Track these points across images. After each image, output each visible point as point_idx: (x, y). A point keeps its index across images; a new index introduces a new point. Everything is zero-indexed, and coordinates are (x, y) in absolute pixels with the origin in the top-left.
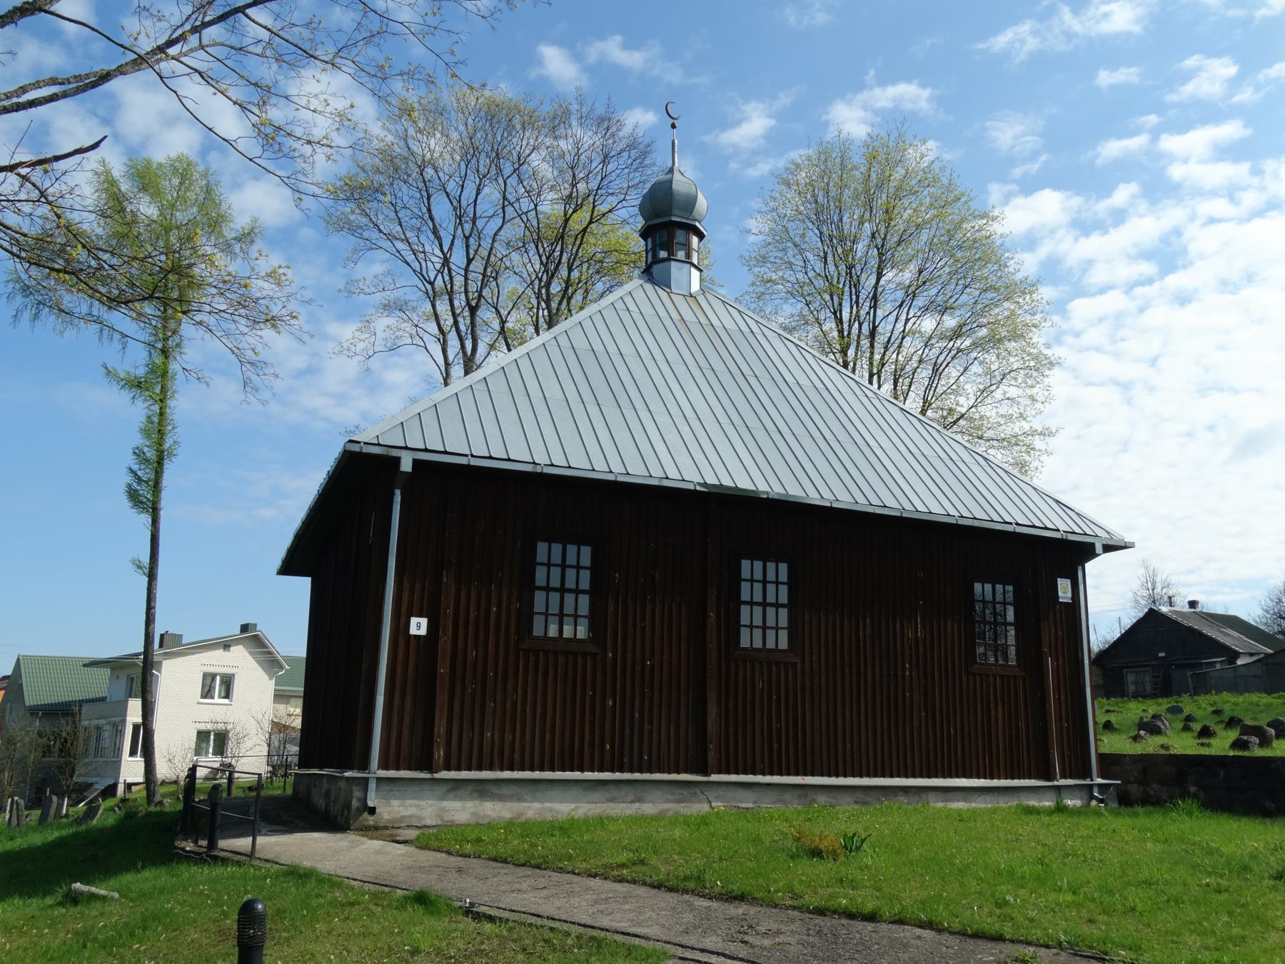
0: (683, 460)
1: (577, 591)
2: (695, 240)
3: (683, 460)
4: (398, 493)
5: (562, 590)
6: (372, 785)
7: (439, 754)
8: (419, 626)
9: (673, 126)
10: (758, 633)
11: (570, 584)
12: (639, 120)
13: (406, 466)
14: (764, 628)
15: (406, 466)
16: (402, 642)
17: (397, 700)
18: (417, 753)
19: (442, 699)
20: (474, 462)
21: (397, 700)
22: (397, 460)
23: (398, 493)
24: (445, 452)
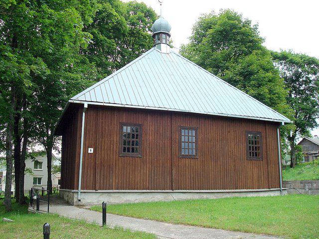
0: (171, 104)
1: (185, 142)
2: (168, 37)
3: (171, 104)
4: (84, 113)
5: (188, 142)
6: (79, 193)
7: (98, 185)
8: (91, 150)
9: (161, 5)
10: (187, 150)
11: (190, 141)
12: (285, 193)
13: (86, 106)
14: (188, 149)
15: (86, 106)
16: (87, 155)
17: (86, 171)
18: (93, 186)
19: (98, 171)
20: (105, 104)
21: (86, 171)
22: (83, 105)
23: (84, 113)
24: (97, 102)
